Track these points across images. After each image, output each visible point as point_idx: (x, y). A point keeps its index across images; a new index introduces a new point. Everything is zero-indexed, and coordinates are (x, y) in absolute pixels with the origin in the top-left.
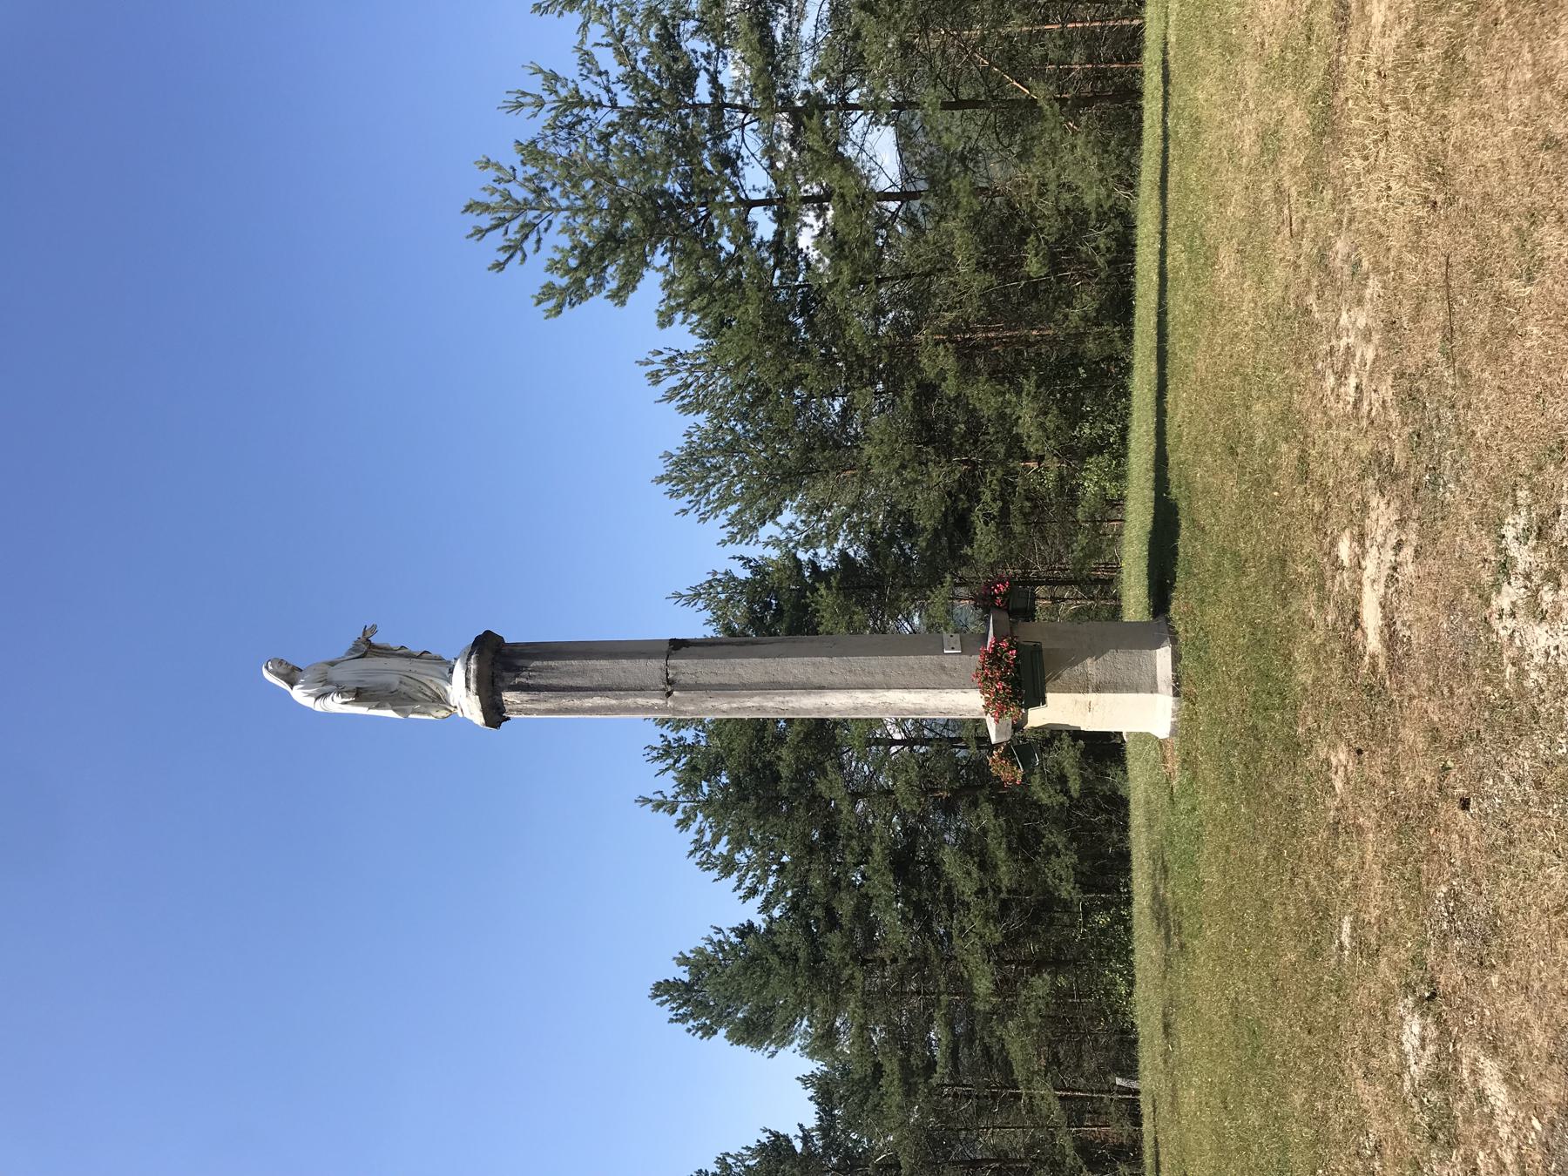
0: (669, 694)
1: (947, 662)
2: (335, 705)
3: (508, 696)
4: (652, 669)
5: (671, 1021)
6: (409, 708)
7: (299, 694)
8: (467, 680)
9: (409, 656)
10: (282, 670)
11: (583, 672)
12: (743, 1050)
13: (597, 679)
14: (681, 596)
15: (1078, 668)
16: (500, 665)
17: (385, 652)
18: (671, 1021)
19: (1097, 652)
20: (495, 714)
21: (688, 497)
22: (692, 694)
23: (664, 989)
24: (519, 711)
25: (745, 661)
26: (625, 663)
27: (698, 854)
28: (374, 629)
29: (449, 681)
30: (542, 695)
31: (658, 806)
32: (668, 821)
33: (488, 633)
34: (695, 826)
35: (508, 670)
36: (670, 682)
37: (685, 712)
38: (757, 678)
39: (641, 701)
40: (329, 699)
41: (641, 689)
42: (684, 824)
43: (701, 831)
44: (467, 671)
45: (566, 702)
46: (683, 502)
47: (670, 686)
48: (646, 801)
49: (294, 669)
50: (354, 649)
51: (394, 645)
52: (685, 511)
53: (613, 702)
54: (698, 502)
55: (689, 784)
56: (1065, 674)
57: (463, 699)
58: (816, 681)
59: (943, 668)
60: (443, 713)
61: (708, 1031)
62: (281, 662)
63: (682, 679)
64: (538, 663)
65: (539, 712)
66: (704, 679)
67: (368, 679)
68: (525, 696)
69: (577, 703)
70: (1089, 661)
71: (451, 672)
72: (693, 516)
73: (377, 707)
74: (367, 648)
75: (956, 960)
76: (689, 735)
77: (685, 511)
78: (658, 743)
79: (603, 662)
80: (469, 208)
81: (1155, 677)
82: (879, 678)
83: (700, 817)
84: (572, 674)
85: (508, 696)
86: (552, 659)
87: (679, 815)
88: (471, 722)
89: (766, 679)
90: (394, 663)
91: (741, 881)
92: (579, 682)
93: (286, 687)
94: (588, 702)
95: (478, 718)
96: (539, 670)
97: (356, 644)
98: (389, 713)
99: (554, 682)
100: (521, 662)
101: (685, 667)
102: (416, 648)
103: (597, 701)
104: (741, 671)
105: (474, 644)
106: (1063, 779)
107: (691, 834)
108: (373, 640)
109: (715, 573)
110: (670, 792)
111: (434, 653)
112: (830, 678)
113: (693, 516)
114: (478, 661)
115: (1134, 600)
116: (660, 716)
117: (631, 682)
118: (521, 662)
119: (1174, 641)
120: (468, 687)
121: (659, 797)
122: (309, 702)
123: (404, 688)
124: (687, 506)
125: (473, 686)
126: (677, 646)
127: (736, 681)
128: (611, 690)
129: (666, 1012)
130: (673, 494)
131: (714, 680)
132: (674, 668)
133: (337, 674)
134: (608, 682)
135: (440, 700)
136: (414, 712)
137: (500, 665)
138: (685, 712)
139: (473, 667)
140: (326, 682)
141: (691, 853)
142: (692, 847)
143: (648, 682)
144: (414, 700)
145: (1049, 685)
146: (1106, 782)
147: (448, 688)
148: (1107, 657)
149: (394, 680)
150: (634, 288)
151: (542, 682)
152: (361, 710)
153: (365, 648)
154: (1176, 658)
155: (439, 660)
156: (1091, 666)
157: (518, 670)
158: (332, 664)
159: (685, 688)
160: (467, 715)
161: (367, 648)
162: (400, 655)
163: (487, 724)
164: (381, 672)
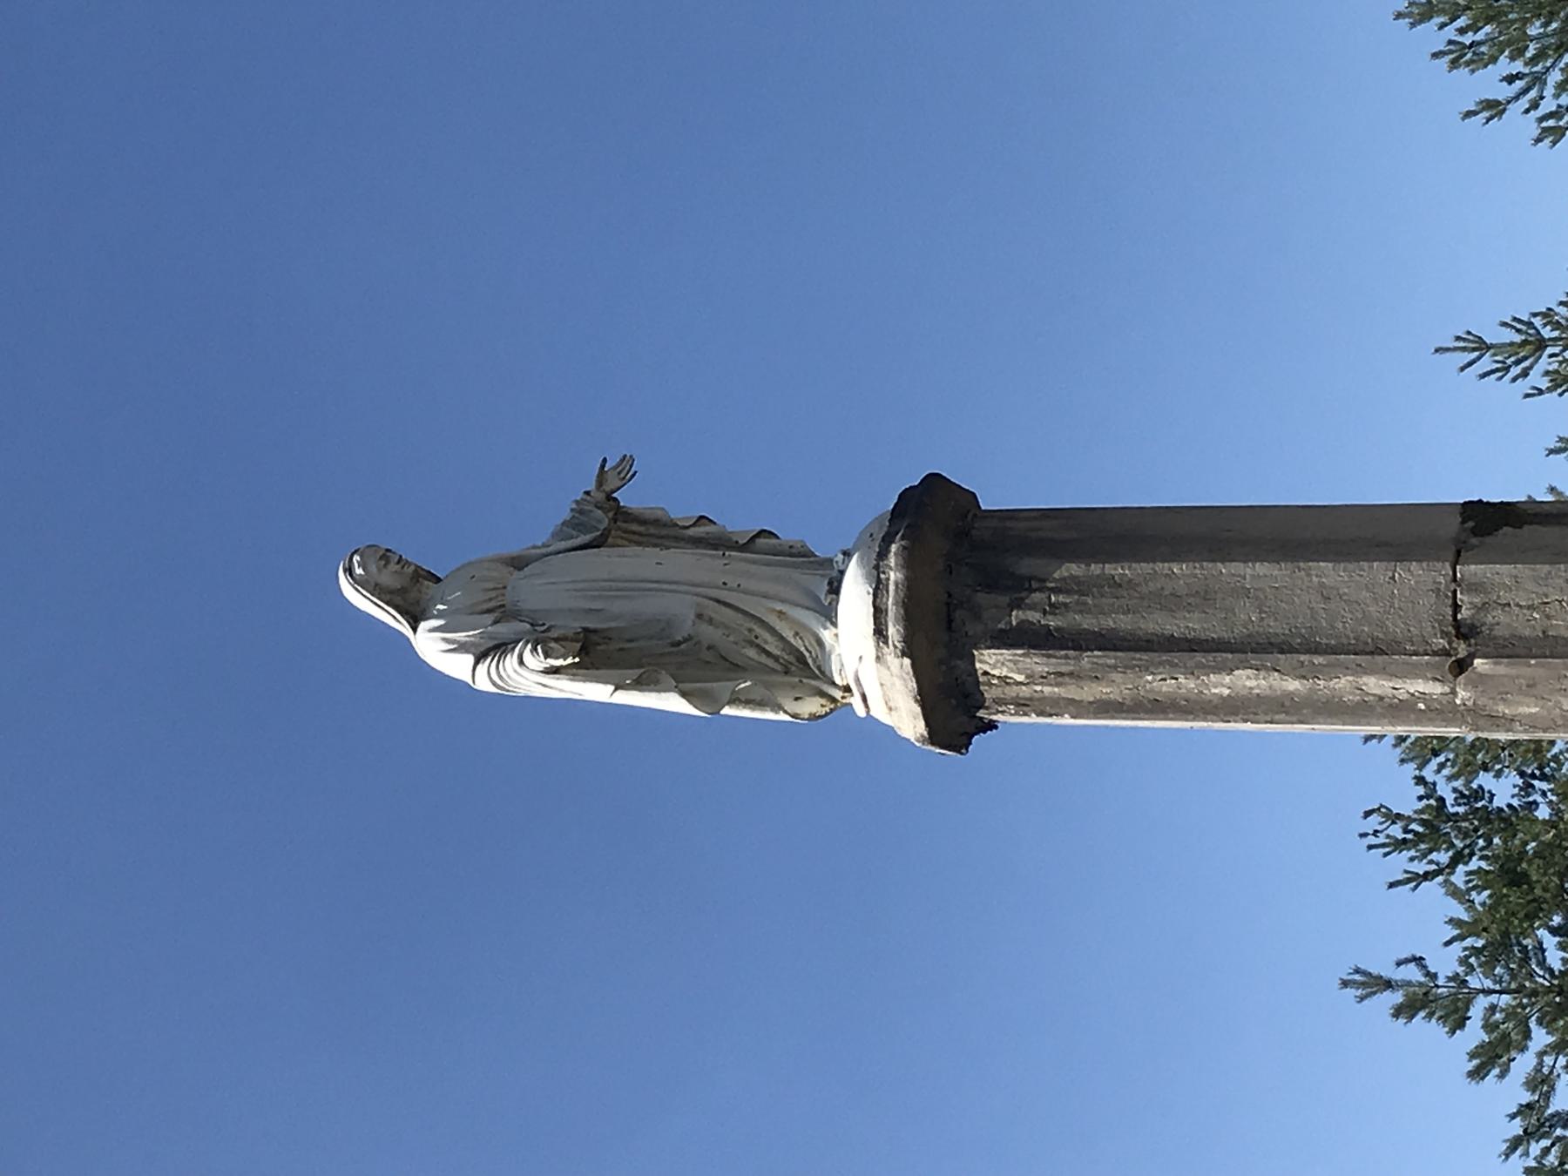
0: (1461, 667)
2: (526, 675)
3: (992, 662)
4: (1410, 590)
6: (723, 688)
7: (431, 645)
8: (879, 613)
9: (720, 543)
10: (387, 579)
11: (1204, 597)
13: (1247, 619)
14: (1482, 346)
16: (976, 574)
17: (655, 531)
20: (955, 711)
21: (1505, 66)
22: (1532, 669)
24: (1023, 705)
26: (1328, 573)
27: (1535, 1148)
28: (626, 469)
29: (829, 615)
30: (1088, 659)
32: (1445, 1050)
33: (934, 482)
34: (1523, 1064)
35: (991, 586)
36: (1463, 631)
37: (1509, 722)
39: (1375, 685)
40: (511, 661)
41: (1376, 650)
42: (1489, 1059)
45: (1158, 683)
46: (1489, 82)
47: (1464, 641)
48: (1375, 984)
49: (423, 576)
50: (578, 521)
51: (681, 512)
52: (1494, 108)
53: (1293, 685)
54: (1539, 80)
55: (1497, 941)
57: (869, 670)
60: (812, 706)
62: (386, 556)
63: (1500, 622)
64: (1073, 569)
65: (1079, 708)
67: (617, 607)
68: (1038, 663)
69: (1188, 684)
71: (835, 589)
72: (1520, 124)
73: (639, 684)
74: (608, 521)
76: (1503, 790)
77: (1494, 108)
78: (1408, 801)
79: (1262, 568)
80: (1437, 351)
83: (1541, 1037)
84: (1172, 602)
85: (992, 662)
86: (1115, 558)
87: (1474, 1034)
88: (890, 731)
90: (680, 563)
93: (405, 629)
94: (1220, 685)
95: (909, 722)
97: (579, 510)
99: (1122, 622)
100: (1027, 566)
101: (1510, 587)
102: (738, 523)
103: (1247, 680)
105: (897, 513)
107: (1509, 1090)
108: (625, 497)
110: (1445, 963)
111: (788, 534)
113: (1520, 124)
114: (910, 562)
116: (1415, 731)
118: (1027, 566)
120: (880, 633)
121: (1412, 973)
122: (458, 666)
123: (708, 633)
124: (1504, 92)
125: (893, 631)
126: (1486, 524)
128: (1285, 648)
130: (1459, 56)
132: (1474, 587)
133: (531, 591)
134: (1275, 627)
135: (806, 669)
136: (734, 700)
137: (976, 574)
138: (1509, 722)
139: (894, 577)
140: (504, 613)
141: (1515, 1144)
142: (1517, 1127)
143: (1396, 628)
144: (736, 669)
147: (827, 635)
149: (680, 609)
150: (1486, 66)
151: (1088, 623)
152: (597, 692)
153: (603, 519)
155: (800, 555)
157: (1018, 588)
158: (518, 563)
159: (1509, 649)
160: (879, 712)
161: (608, 521)
162: (697, 542)
163: (936, 735)
164: (660, 593)
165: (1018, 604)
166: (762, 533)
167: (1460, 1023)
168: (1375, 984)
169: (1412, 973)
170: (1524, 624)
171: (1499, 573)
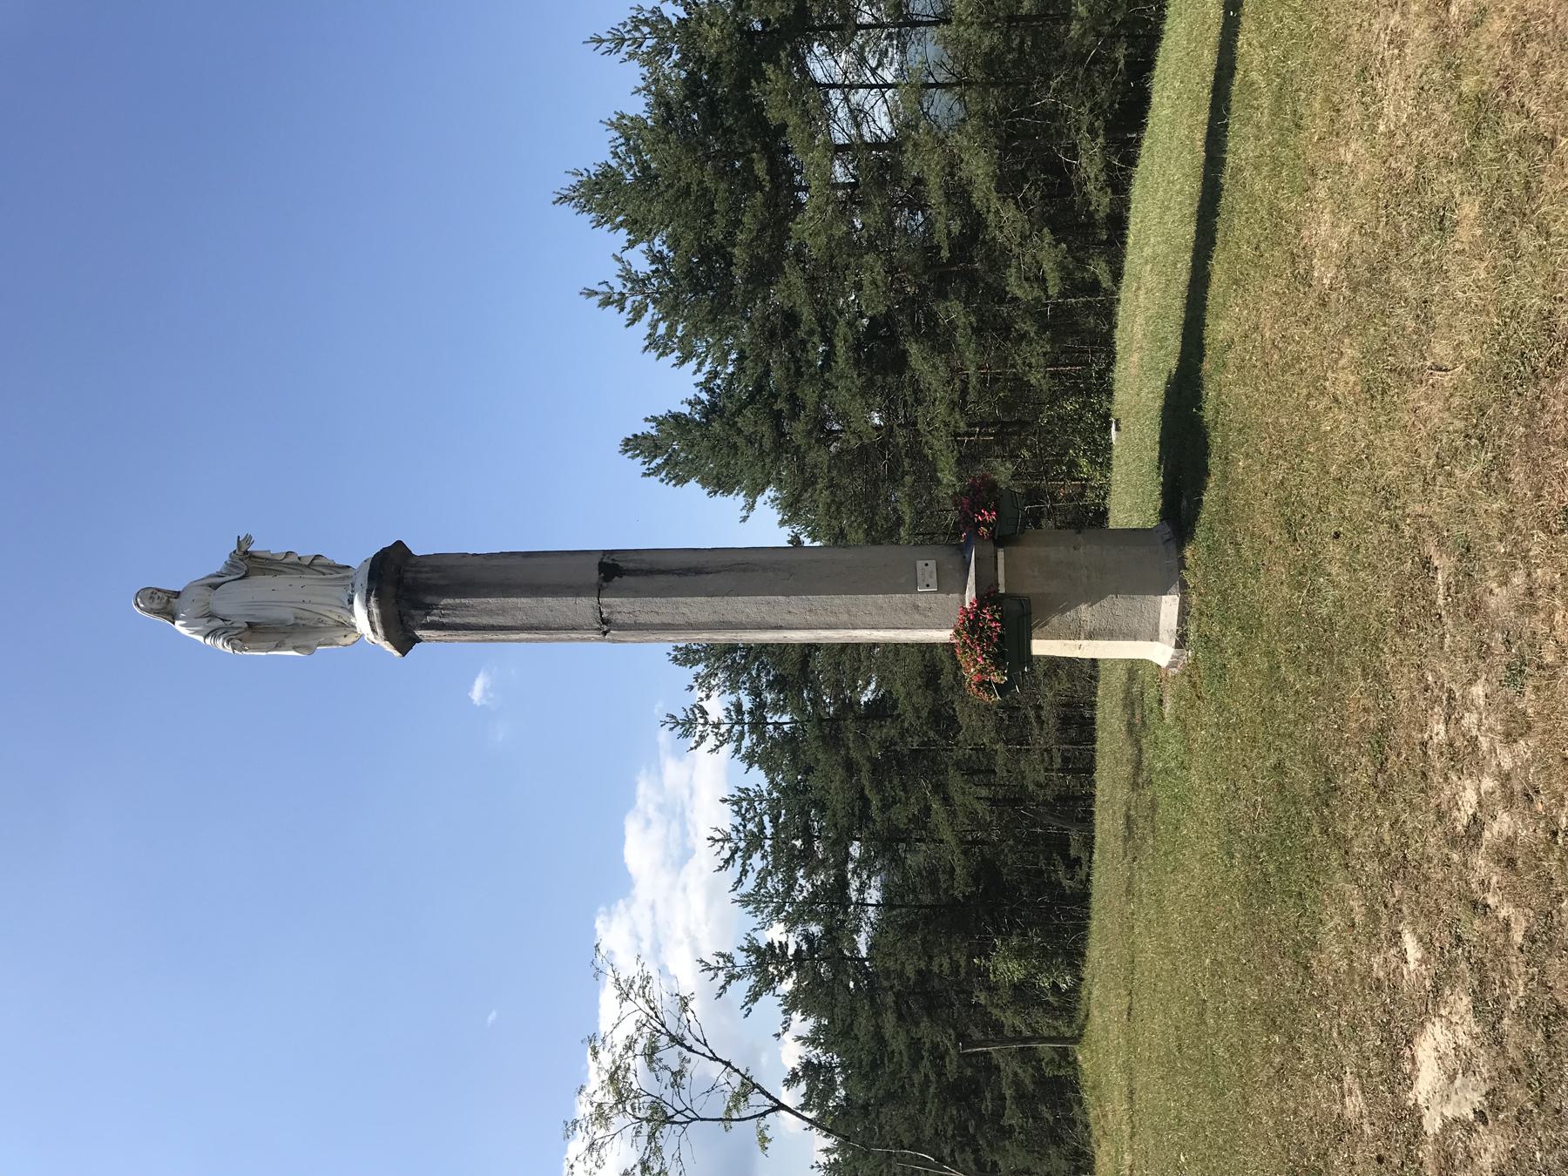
1: (922, 601)
5: (645, 475)
11: (503, 611)
12: (719, 498)
13: (520, 618)
14: (601, 41)
15: (1071, 614)
18: (645, 475)
19: (1093, 597)
23: (634, 445)
25: (689, 600)
29: (351, 611)
31: (606, 302)
34: (647, 318)
35: (416, 608)
36: (605, 622)
38: (704, 617)
43: (654, 326)
44: (370, 614)
48: (593, 293)
50: (232, 566)
56: (1055, 620)
58: (772, 620)
59: (916, 607)
61: (681, 481)
63: (619, 618)
66: (643, 619)
70: (1083, 607)
74: (248, 563)
75: (940, 893)
81: (1157, 624)
82: (844, 617)
84: (490, 613)
89: (716, 618)
91: (700, 364)
92: (500, 621)
96: (454, 608)
98: (293, 653)
99: (472, 620)
100: (429, 599)
103: (524, 636)
104: (685, 610)
106: (1042, 281)
107: (643, 327)
109: (640, 9)
112: (788, 617)
114: (380, 605)
115: (1132, 498)
117: (561, 621)
118: (429, 599)
119: (1184, 585)
121: (604, 288)
127: (680, 620)
129: (637, 465)
131: (657, 620)
134: (534, 621)
137: (411, 592)
139: (375, 611)
143: (579, 620)
145: (1035, 632)
146: (1087, 271)
148: (1105, 602)
151: (458, 620)
154: (1184, 613)
156: (1085, 612)
157: (428, 609)
159: (622, 627)
161: (248, 563)
165: (428, 614)
166: (318, 556)
167: (622, 310)
168: (593, 293)
169: (604, 288)
170: (628, 619)
171: (614, 601)
